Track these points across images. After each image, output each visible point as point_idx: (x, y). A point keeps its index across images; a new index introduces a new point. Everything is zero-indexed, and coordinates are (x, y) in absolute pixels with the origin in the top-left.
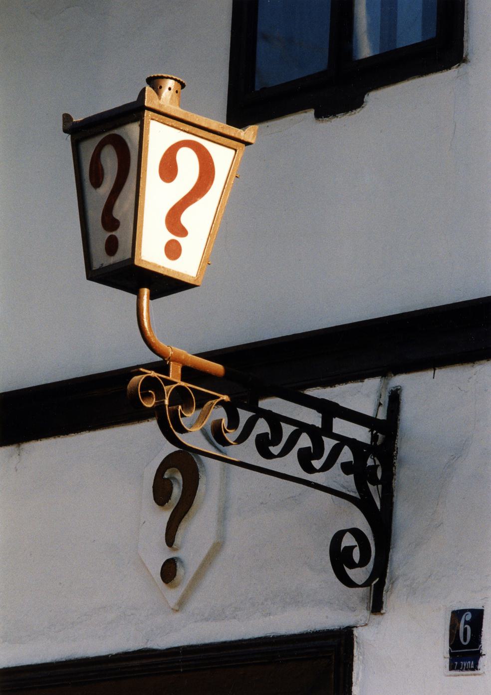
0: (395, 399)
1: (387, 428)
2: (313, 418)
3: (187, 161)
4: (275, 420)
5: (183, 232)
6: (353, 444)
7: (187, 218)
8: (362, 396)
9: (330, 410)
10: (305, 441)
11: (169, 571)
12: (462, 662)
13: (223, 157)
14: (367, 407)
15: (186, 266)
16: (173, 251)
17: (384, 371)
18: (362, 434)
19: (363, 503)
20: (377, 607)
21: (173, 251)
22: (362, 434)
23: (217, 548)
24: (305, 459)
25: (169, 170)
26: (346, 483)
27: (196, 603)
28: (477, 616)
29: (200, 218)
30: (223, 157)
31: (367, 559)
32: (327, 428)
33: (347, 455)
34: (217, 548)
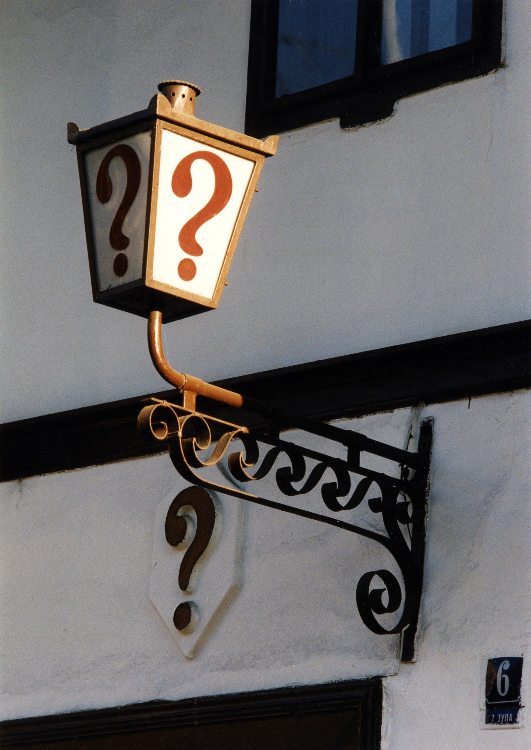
0: (427, 430)
1: (418, 461)
2: (338, 451)
3: (203, 175)
4: (297, 453)
5: (198, 251)
6: (382, 479)
7: (201, 236)
8: (391, 427)
9: (357, 443)
10: (329, 476)
11: (183, 617)
12: (499, 715)
13: (241, 170)
14: (396, 440)
15: (202, 287)
16: (187, 270)
17: (416, 401)
18: (391, 469)
19: (393, 543)
20: (407, 655)
21: (187, 270)
22: (391, 469)
23: (235, 592)
24: (330, 495)
25: (182, 183)
26: (375, 521)
27: (212, 651)
28: (517, 664)
29: (217, 236)
30: (241, 170)
31: (396, 604)
32: (353, 463)
33: (375, 491)
34: (235, 592)
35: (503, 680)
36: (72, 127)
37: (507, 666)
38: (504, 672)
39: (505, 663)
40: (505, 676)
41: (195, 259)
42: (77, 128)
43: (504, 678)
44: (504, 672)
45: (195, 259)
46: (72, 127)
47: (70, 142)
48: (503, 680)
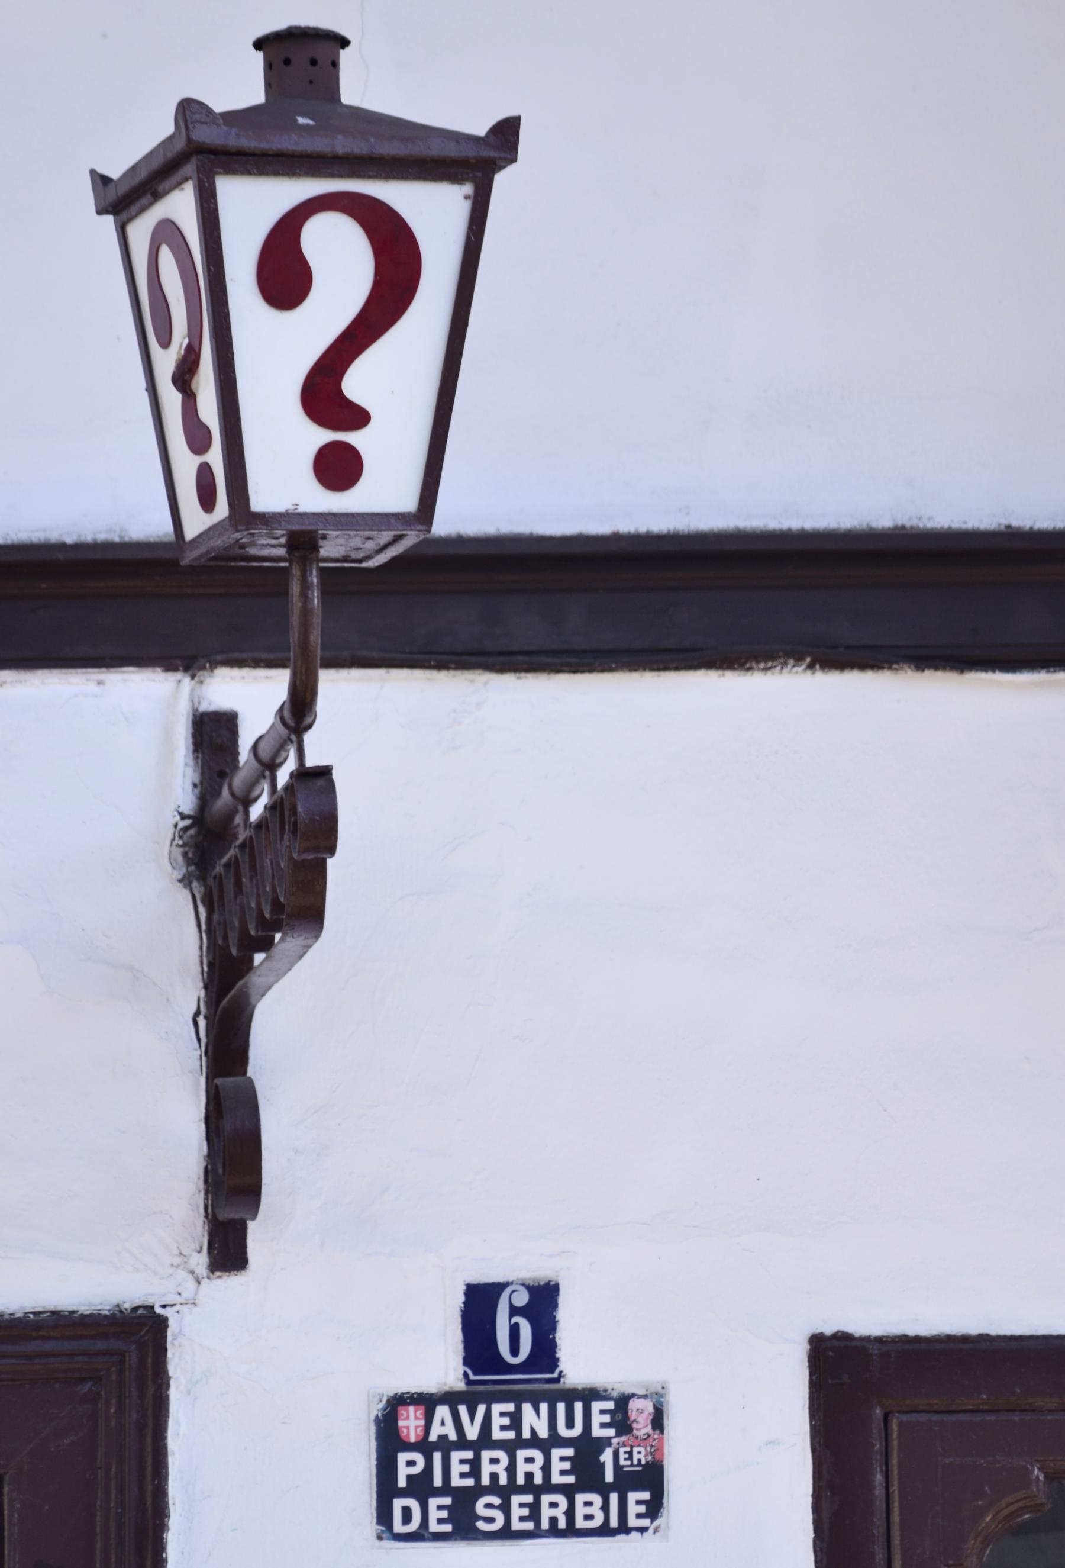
5: (359, 418)
7: (358, 383)
16: (338, 467)
21: (338, 467)
25: (285, 277)
28: (543, 1300)
35: (515, 1331)
36: (101, 181)
37: (522, 1299)
38: (514, 1311)
39: (513, 1292)
40: (516, 1319)
41: (352, 438)
42: (343, 47)
43: (517, 1325)
44: (514, 1311)
45: (352, 438)
46: (101, 181)
47: (100, 212)
48: (515, 1331)
